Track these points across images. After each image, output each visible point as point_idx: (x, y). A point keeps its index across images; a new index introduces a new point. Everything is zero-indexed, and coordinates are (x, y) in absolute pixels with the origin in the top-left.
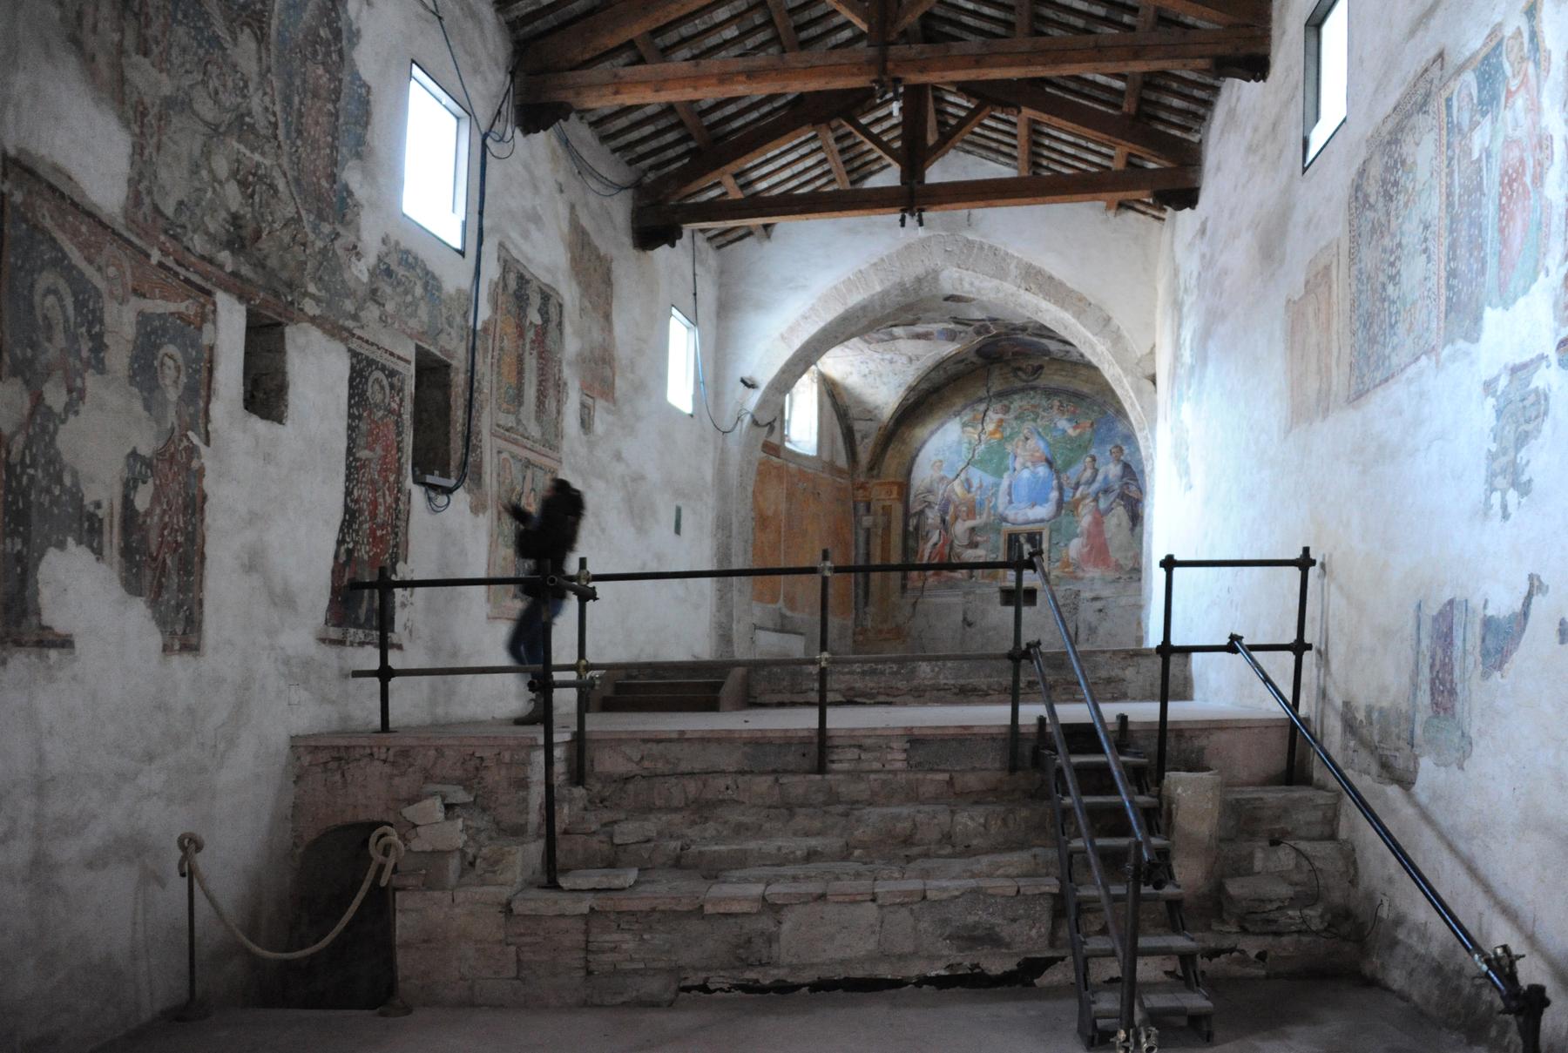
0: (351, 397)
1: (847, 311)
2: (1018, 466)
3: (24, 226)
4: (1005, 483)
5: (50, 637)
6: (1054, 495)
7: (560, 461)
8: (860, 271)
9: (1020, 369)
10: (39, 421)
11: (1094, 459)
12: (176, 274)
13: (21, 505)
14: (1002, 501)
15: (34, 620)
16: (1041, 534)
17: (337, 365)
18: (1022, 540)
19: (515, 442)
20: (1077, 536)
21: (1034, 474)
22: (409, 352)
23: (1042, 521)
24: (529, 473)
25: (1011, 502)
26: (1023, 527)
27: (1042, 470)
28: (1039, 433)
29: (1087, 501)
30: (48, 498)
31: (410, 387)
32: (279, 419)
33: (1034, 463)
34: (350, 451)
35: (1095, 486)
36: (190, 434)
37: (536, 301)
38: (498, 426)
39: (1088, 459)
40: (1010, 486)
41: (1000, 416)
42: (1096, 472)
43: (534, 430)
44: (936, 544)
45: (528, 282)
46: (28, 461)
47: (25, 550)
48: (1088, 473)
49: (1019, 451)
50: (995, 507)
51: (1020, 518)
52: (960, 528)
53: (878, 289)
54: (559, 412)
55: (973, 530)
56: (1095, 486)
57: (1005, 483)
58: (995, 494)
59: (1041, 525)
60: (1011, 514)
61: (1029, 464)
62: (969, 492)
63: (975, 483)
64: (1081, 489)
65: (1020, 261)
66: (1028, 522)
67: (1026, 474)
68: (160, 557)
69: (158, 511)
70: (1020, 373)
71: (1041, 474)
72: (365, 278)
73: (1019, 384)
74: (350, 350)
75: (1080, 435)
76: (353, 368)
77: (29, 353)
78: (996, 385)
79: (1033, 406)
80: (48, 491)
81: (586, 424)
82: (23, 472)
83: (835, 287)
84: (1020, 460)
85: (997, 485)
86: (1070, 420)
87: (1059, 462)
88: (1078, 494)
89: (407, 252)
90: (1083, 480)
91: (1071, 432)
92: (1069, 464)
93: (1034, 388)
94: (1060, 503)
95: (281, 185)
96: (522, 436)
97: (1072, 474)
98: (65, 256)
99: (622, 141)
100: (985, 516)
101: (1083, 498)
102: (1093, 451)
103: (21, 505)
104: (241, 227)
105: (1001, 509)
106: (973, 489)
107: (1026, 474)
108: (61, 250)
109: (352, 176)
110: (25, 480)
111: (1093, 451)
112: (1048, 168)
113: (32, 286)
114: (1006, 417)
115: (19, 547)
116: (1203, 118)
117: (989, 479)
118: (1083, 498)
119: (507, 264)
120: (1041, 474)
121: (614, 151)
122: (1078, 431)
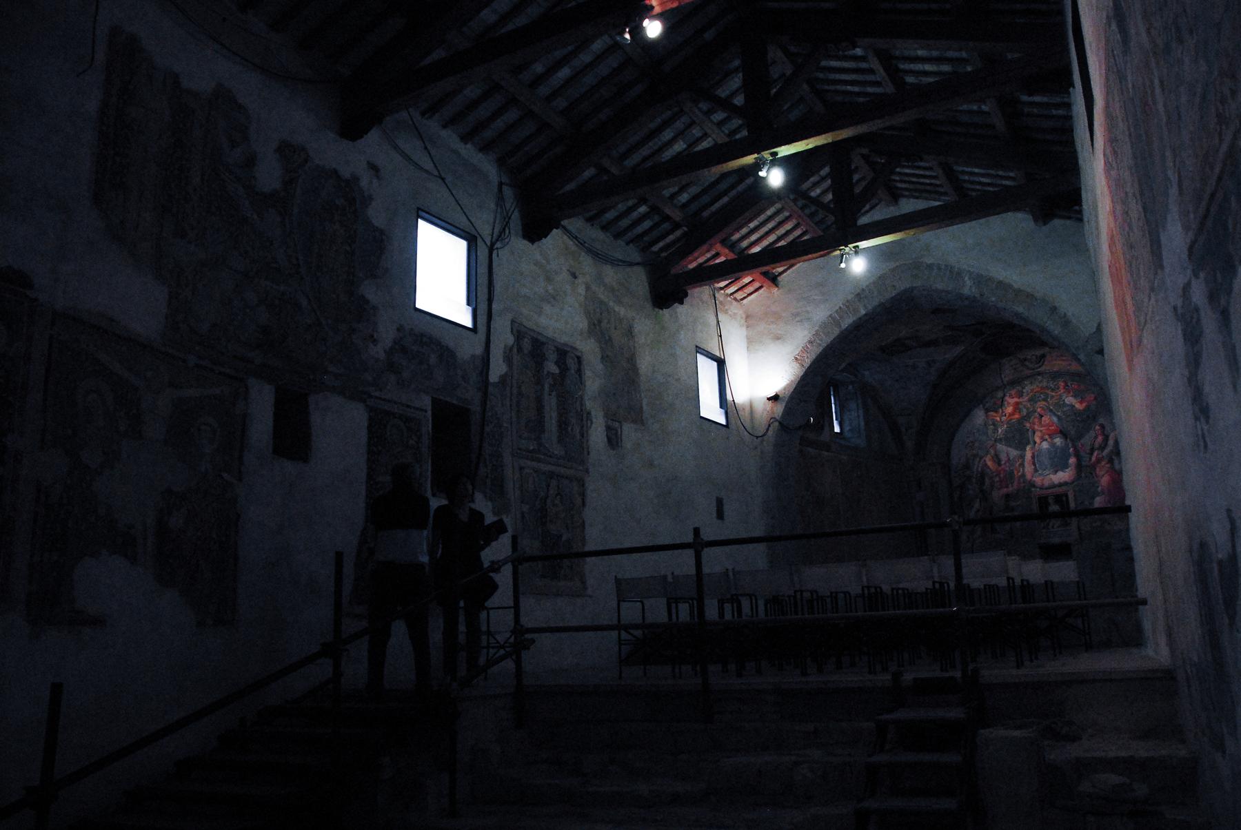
0: (370, 439)
1: (842, 332)
2: (1037, 440)
4: (1028, 455)
6: (1072, 460)
7: (587, 471)
8: (848, 301)
9: (1025, 360)
11: (1102, 427)
14: (1028, 469)
16: (1067, 496)
17: (355, 417)
18: (1050, 501)
19: (539, 461)
20: (1098, 494)
21: (1053, 445)
22: (426, 402)
23: (1066, 483)
24: (554, 483)
25: (1036, 470)
26: (1050, 491)
27: (1058, 441)
28: (1051, 411)
29: (1103, 463)
31: (427, 427)
32: (305, 459)
33: (1051, 436)
34: (370, 477)
35: (1106, 451)
36: (225, 475)
37: (552, 356)
38: (520, 449)
39: (1097, 427)
40: (1033, 457)
41: (1016, 400)
42: (1106, 438)
43: (558, 450)
44: (978, 511)
45: (543, 344)
48: (1100, 438)
49: (1036, 427)
50: (1023, 475)
51: (1046, 483)
52: (996, 495)
53: (863, 312)
54: (582, 436)
55: (1007, 496)
56: (1106, 451)
57: (1028, 455)
58: (1022, 465)
59: (1064, 488)
60: (1038, 480)
61: (1047, 437)
62: (999, 464)
63: (1003, 457)
64: (1095, 454)
65: (970, 273)
66: (1054, 486)
67: (1045, 445)
70: (1027, 363)
71: (1058, 444)
72: (382, 355)
73: (1029, 372)
74: (367, 406)
75: (1088, 407)
76: (370, 419)
78: (1008, 374)
79: (1042, 388)
81: (613, 440)
83: (830, 316)
84: (1038, 434)
85: (1022, 457)
86: (1075, 396)
87: (1073, 432)
88: (1094, 459)
89: (422, 335)
90: (1097, 445)
91: (1078, 406)
92: (1080, 436)
93: (1039, 374)
94: (1079, 466)
95: (304, 303)
96: (544, 454)
97: (1087, 440)
99: (630, 235)
100: (1015, 483)
101: (1099, 460)
102: (1101, 420)
105: (1028, 477)
106: (1003, 462)
107: (1045, 445)
109: (370, 291)
111: (1101, 420)
112: (973, 190)
114: (1021, 400)
117: (1014, 453)
118: (1099, 460)
119: (519, 333)
120: (1058, 444)
121: (628, 244)
122: (1084, 405)
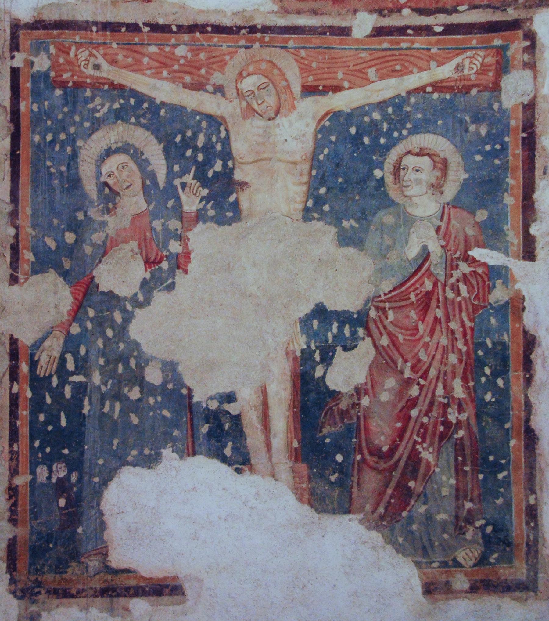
3: (58, 92)
5: (132, 583)
10: (91, 313)
12: (427, 30)
13: (63, 423)
15: (94, 564)
30: (118, 406)
46: (70, 366)
47: (74, 478)
68: (403, 451)
69: (391, 382)
77: (70, 238)
80: (117, 396)
82: (63, 382)
98: (140, 98)
103: (63, 423)
104: (65, 99)
108: (134, 93)
110: (68, 391)
112: (528, 536)
113: (75, 155)
115: (62, 474)
116: (189, 456)
